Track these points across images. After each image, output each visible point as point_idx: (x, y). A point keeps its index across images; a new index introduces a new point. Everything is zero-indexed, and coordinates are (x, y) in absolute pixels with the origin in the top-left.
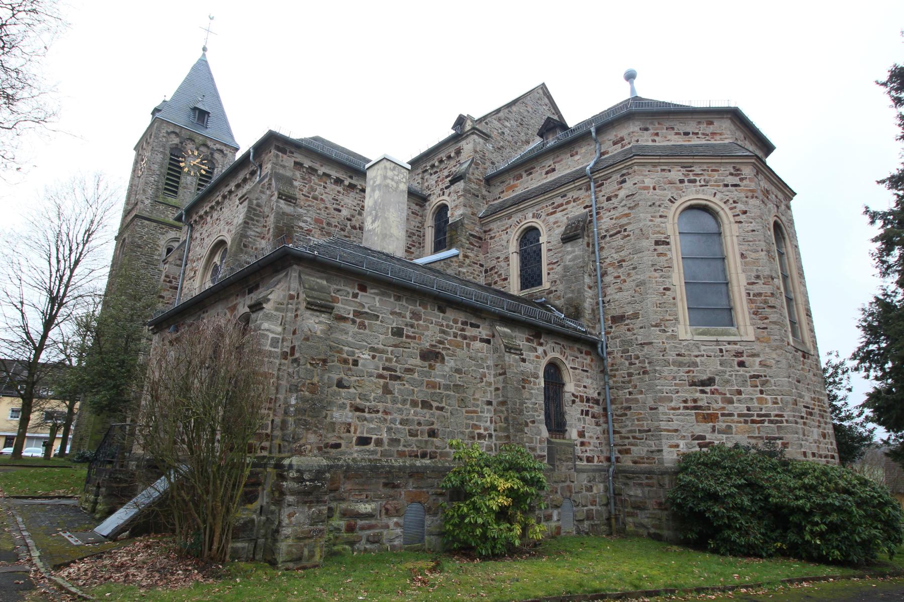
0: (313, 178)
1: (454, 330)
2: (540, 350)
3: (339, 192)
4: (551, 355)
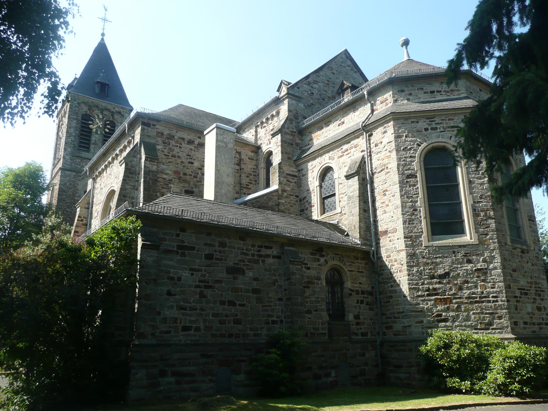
0: (171, 141)
1: (252, 252)
2: (322, 260)
3: (191, 149)
4: (331, 263)
